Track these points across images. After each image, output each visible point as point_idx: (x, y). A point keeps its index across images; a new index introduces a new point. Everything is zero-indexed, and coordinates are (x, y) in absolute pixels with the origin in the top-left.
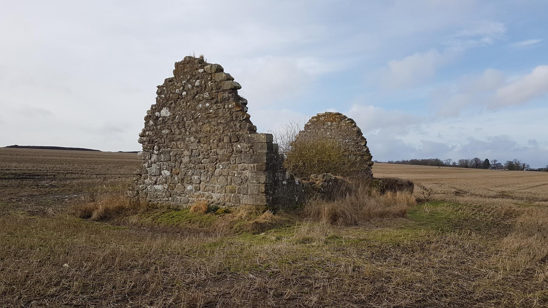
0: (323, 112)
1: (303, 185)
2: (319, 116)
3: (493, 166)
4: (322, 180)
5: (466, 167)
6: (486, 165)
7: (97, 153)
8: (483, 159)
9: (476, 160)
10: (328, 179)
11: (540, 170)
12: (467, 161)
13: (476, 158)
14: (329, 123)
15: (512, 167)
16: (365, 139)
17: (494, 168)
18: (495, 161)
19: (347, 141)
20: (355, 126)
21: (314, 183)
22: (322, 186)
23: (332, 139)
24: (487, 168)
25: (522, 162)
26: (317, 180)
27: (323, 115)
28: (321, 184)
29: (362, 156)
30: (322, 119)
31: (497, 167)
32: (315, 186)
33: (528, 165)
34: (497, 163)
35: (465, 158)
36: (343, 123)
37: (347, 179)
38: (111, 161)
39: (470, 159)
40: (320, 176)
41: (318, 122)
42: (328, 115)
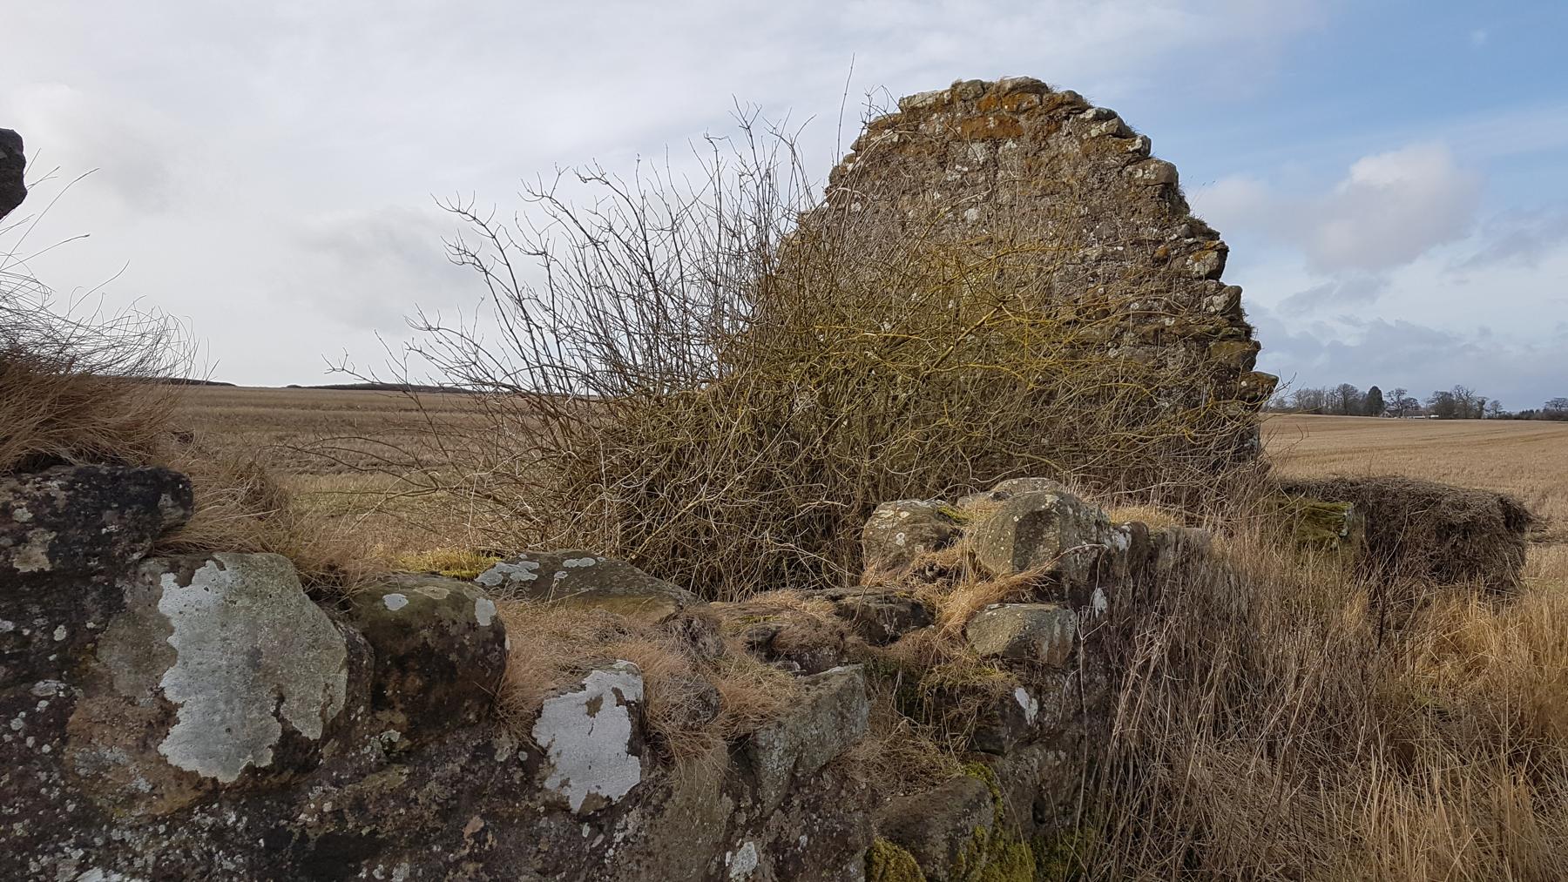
0: (940, 84)
1: (744, 751)
2: (913, 112)
3: (1393, 408)
4: (1004, 573)
5: (1318, 412)
6: (1373, 404)
7: (209, 390)
8: (1364, 388)
9: (1346, 390)
10: (1081, 550)
11: (1527, 416)
12: (1318, 394)
13: (1345, 386)
14: (979, 152)
15: (1450, 408)
16: (1213, 235)
17: (1397, 413)
18: (1400, 392)
19: (1094, 253)
20: (1143, 155)
21: (921, 615)
22: (1018, 656)
23: (1008, 237)
24: (1377, 414)
25: (1478, 394)
26: (947, 576)
27: (942, 104)
28: (1003, 627)
29: (1202, 340)
30: (935, 125)
31: (1406, 409)
32: (926, 659)
33: (1496, 404)
34: (1403, 397)
35: (1314, 385)
36: (1066, 145)
37: (1210, 533)
38: (245, 416)
39: (1328, 389)
40: (983, 514)
41: (905, 146)
42: (971, 99)
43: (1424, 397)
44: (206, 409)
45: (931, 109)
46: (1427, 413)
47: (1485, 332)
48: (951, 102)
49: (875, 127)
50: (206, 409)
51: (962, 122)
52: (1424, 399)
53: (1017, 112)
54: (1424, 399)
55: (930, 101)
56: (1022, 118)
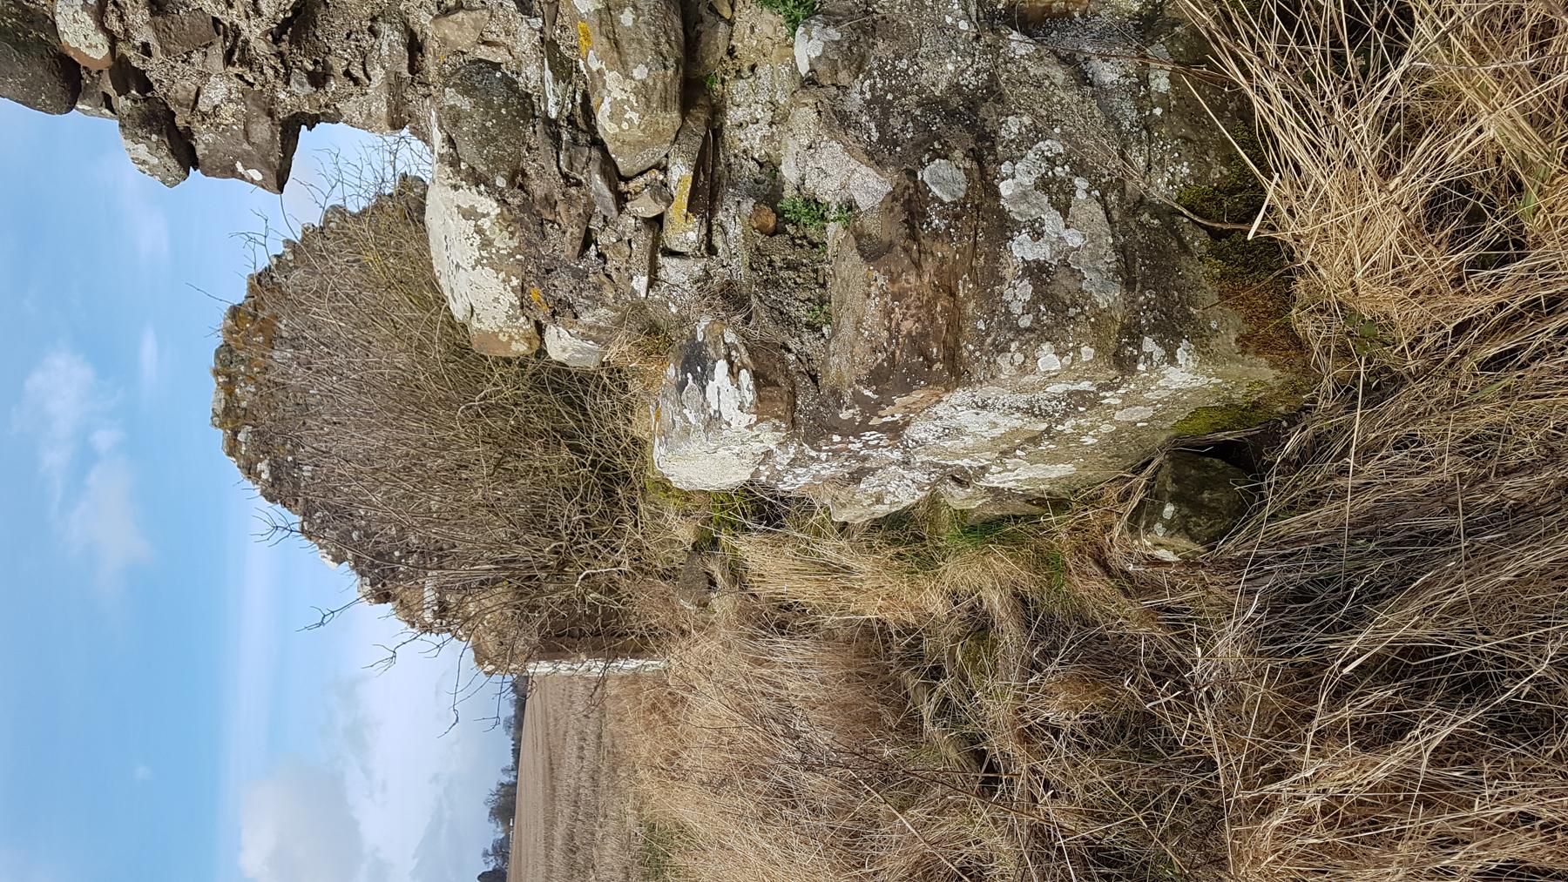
2: (230, 416)
11: (516, 752)
14: (282, 354)
15: (505, 807)
18: (486, 854)
24: (505, 874)
27: (229, 386)
31: (501, 850)
33: (504, 770)
42: (228, 364)
43: (492, 832)
44: (1385, 92)
45: (230, 393)
46: (508, 829)
47: (436, 778)
48: (228, 376)
49: (232, 450)
50: (1385, 92)
51: (249, 367)
52: (494, 832)
53: (255, 317)
54: (494, 832)
55: (222, 395)
56: (261, 315)
